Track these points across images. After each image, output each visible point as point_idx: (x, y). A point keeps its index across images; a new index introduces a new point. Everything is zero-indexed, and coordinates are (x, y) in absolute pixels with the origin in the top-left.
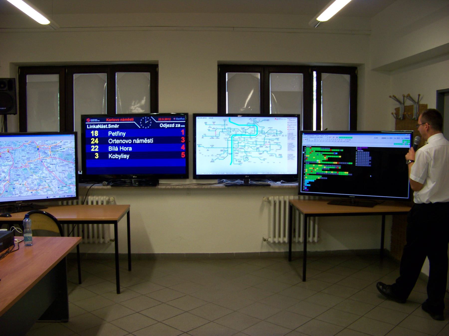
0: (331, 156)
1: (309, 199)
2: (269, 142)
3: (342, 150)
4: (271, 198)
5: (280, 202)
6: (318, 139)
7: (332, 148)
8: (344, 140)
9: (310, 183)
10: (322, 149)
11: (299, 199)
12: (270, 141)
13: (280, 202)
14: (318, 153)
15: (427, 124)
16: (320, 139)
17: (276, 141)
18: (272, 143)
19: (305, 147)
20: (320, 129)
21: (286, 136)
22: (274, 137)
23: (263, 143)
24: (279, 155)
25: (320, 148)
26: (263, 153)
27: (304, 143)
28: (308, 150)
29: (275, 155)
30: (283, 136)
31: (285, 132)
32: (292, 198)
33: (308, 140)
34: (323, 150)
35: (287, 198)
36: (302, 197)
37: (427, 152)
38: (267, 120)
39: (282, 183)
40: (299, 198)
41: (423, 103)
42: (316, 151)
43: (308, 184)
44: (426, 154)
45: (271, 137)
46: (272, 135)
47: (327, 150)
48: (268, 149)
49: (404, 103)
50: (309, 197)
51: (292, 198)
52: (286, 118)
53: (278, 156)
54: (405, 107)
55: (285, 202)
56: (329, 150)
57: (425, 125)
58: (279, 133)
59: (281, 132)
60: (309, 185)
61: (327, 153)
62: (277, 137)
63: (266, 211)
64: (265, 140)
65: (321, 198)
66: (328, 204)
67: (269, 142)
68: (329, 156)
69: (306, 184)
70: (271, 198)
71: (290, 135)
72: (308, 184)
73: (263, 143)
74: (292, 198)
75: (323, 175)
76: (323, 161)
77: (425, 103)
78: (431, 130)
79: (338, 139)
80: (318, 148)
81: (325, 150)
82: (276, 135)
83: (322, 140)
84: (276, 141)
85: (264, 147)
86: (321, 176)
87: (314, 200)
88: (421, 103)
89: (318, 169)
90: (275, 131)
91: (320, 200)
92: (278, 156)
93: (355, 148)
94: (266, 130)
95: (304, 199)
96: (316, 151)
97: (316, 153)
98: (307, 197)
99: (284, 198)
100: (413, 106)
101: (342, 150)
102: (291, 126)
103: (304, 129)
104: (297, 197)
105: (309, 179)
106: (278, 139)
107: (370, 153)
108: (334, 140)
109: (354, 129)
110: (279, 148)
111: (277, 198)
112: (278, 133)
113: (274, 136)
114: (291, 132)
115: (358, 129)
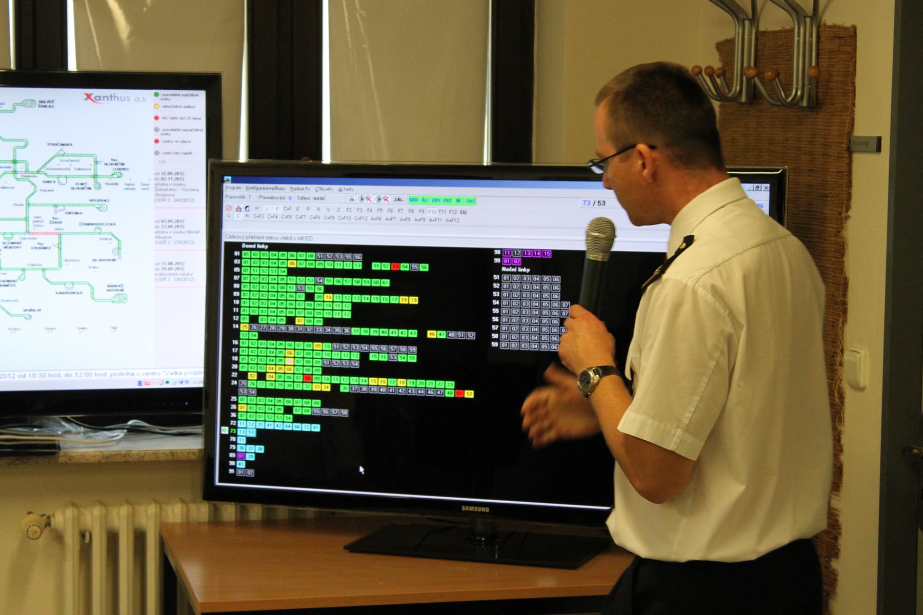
0: (365, 299)
1: (269, 523)
2: (55, 221)
3: (424, 267)
4: (63, 518)
5: (112, 538)
6: (303, 205)
7: (371, 253)
8: (432, 210)
9: (263, 436)
10: (318, 262)
11: (215, 521)
12: (61, 216)
13: (112, 538)
14: (301, 280)
15: (642, 147)
16: (314, 205)
17: (92, 214)
18: (70, 223)
19: (237, 246)
20: (319, 156)
21: (145, 187)
22: (83, 196)
23: (21, 226)
24: (111, 288)
25: (311, 255)
26: (22, 278)
27: (231, 232)
28: (248, 261)
29: (86, 290)
30: (130, 187)
31: (143, 166)
32: (182, 511)
33: (266, 212)
34: (328, 265)
35: (148, 516)
36: (229, 511)
37: (715, 290)
38: (43, 104)
39: (133, 430)
40: (216, 512)
41: (839, 22)
42: (292, 272)
43: (250, 441)
44: (710, 297)
45: (63, 194)
46: (72, 182)
47: (348, 266)
48: (49, 258)
49: (754, 19)
50: (243, 512)
51: (175, 513)
52: (148, 94)
53: (101, 292)
54: (759, 35)
55: (140, 538)
56: (358, 266)
57: (634, 152)
58: (110, 170)
59: (119, 167)
60: (260, 449)
61: (347, 282)
62: (94, 194)
63: (41, 583)
64: (33, 212)
65: (329, 515)
66: (352, 548)
67: (55, 221)
68: (357, 298)
69: (242, 440)
70: (63, 518)
71: (166, 184)
72: (250, 441)
73: (21, 226)
74: (175, 513)
75: (332, 398)
76: (328, 322)
77: (848, 24)
78: (673, 179)
79: (406, 205)
80: (302, 255)
81: (339, 265)
82: (90, 182)
83: (323, 213)
84: (92, 214)
85: (27, 244)
86: (317, 403)
87: (296, 524)
88: (831, 18)
89: (294, 365)
90: (87, 162)
91: (322, 525)
92: (101, 292)
93: (489, 253)
94: (34, 157)
95: (243, 522)
96: (292, 272)
97: (293, 279)
98: (256, 511)
99: (105, 518)
100: (791, 31)
101: (424, 267)
102: (174, 136)
103: (252, 153)
104: (202, 511)
105: (254, 417)
106: (101, 203)
107: (563, 284)
108: (385, 215)
109: (515, 157)
110: (106, 249)
111: (93, 518)
112: (103, 170)
113: (82, 187)
114: (173, 164)
115: (540, 157)
